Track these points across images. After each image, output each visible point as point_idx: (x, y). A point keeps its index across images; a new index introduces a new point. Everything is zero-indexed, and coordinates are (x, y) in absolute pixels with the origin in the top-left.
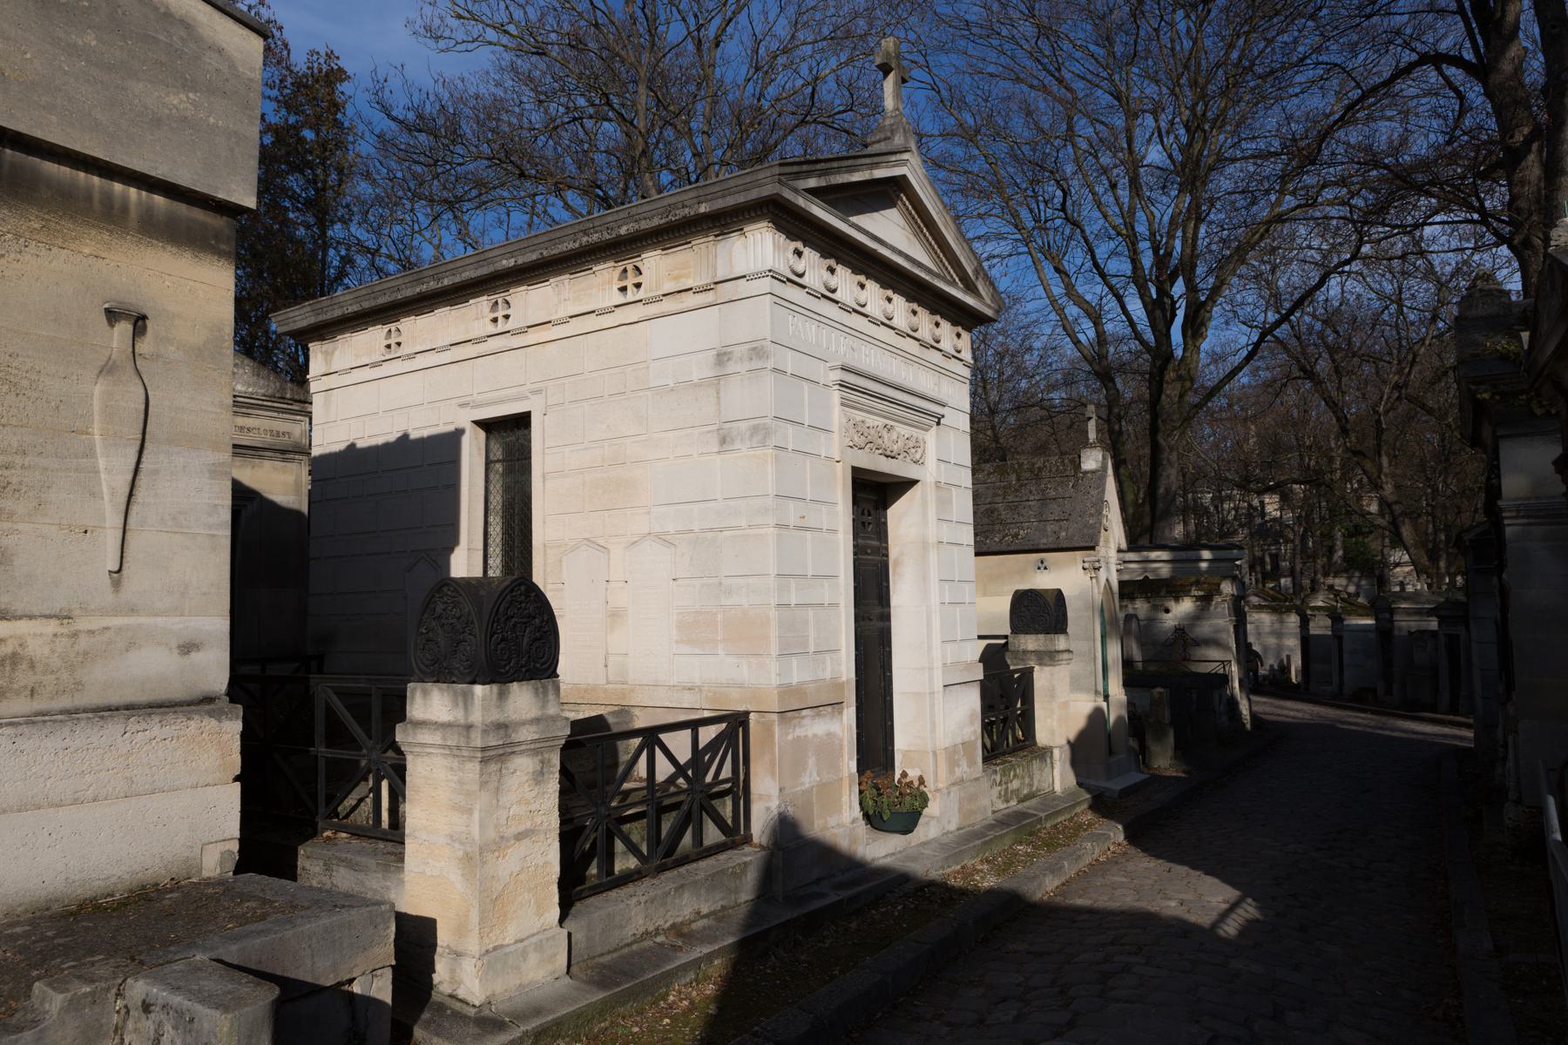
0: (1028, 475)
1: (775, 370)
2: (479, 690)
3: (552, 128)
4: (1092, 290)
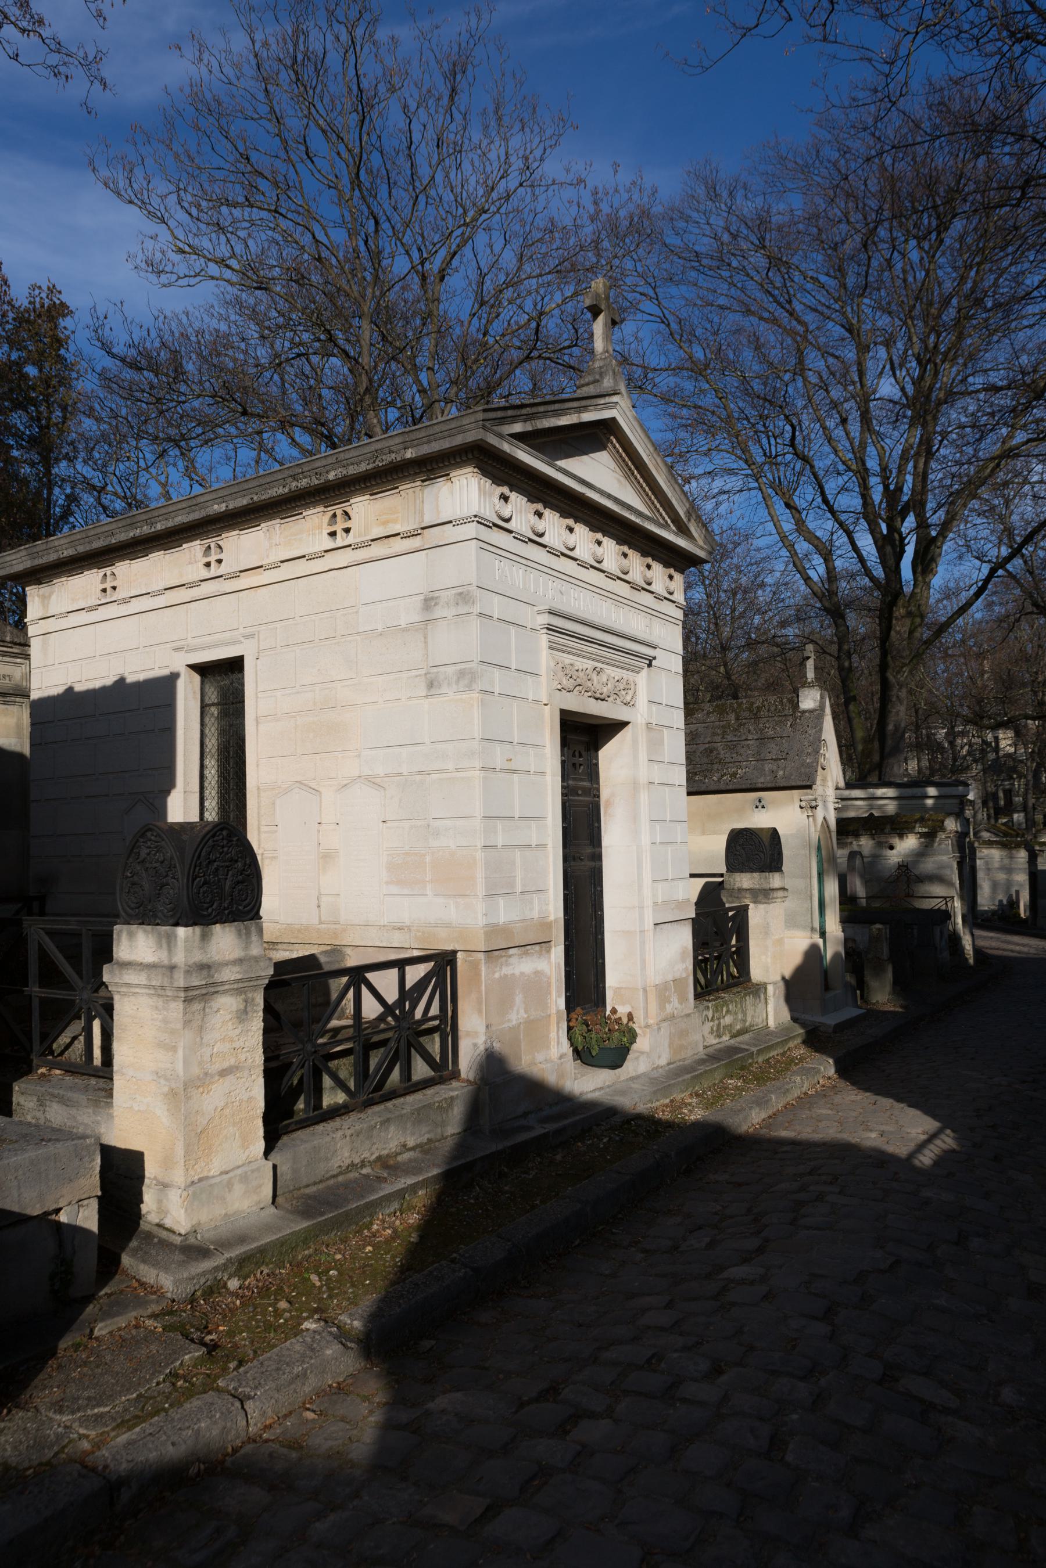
0: (747, 714)
1: (481, 615)
2: (181, 931)
3: (278, 364)
4: (822, 526)
